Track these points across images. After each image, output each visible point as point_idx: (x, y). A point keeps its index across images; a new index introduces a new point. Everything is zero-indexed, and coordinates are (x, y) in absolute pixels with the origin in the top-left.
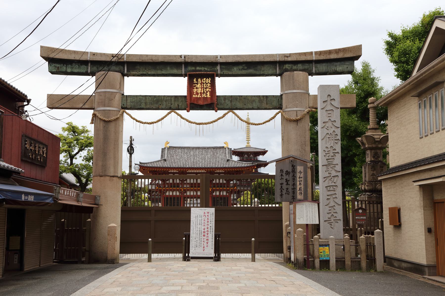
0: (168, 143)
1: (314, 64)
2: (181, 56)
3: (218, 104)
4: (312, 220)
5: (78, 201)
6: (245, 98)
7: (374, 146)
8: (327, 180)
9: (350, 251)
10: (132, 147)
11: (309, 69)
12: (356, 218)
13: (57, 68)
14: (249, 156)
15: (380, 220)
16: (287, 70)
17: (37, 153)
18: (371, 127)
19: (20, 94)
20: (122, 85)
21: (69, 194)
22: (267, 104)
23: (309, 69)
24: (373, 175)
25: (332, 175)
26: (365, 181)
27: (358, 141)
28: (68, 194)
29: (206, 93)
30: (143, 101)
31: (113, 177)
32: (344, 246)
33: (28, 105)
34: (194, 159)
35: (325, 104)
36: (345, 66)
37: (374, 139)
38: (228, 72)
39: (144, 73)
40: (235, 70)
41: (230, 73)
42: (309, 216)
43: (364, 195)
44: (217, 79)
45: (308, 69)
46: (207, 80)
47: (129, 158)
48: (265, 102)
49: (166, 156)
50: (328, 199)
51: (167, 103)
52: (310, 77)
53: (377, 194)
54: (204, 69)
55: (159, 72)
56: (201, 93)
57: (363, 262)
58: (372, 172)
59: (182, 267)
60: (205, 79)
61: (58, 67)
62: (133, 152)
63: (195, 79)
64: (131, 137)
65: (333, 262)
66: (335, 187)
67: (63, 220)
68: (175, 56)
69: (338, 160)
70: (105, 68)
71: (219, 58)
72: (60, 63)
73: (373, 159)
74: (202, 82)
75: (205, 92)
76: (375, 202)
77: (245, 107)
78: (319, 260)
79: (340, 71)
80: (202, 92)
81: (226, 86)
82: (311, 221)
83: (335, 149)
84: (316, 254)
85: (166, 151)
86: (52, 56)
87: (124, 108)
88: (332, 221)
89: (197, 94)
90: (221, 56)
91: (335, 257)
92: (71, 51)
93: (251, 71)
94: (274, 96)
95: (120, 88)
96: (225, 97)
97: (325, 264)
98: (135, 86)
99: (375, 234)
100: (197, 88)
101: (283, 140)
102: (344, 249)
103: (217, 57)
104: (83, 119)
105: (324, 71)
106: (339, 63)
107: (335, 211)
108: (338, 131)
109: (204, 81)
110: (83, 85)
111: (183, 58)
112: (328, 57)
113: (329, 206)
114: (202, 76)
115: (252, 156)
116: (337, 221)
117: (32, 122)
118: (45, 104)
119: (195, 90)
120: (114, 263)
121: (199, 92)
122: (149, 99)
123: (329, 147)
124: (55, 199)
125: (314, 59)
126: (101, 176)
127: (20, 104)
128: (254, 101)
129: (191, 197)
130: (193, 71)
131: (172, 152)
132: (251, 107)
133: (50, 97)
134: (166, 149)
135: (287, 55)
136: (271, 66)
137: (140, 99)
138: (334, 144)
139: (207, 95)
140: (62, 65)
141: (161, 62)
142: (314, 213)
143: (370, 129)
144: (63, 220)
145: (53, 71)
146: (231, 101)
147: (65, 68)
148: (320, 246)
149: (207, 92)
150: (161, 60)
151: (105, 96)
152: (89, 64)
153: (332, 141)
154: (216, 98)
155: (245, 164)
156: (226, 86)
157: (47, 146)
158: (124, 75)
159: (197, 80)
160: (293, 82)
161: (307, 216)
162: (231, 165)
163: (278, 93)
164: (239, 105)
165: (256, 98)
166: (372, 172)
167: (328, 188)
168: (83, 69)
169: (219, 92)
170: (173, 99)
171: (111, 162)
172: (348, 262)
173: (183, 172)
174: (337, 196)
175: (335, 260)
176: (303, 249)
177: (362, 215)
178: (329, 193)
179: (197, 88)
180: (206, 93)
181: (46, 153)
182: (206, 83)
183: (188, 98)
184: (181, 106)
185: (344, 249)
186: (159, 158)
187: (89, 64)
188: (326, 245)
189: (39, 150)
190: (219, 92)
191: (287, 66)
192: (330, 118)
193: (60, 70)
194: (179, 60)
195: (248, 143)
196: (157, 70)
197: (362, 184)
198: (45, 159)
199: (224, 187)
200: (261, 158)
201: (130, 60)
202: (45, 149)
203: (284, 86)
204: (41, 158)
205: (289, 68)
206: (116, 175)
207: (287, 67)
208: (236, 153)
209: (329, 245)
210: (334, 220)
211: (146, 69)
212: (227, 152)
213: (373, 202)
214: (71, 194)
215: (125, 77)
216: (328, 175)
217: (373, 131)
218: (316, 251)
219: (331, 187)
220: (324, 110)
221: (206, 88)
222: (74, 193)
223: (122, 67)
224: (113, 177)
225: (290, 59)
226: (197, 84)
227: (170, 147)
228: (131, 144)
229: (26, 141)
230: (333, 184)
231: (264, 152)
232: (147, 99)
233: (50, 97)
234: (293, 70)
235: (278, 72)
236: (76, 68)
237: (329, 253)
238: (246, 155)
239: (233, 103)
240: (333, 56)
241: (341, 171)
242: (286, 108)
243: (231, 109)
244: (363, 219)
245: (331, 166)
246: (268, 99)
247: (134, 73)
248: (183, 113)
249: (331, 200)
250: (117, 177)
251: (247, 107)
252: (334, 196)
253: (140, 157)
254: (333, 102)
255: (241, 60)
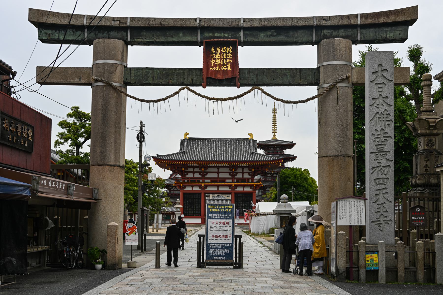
0: (187, 134)
1: (359, 29)
2: (196, 19)
3: (241, 79)
4: (358, 221)
5: (68, 195)
6: (273, 72)
7: (428, 131)
8: (376, 171)
9: (404, 258)
10: (143, 134)
11: (353, 36)
12: (413, 218)
13: (48, 35)
14: (275, 149)
15: (436, 220)
16: (325, 37)
17: (19, 135)
18: (425, 109)
19: (5, 67)
20: (125, 56)
21: (55, 186)
22: (301, 79)
23: (353, 36)
24: (426, 166)
25: (382, 165)
26: (417, 173)
27: (408, 125)
28: (54, 185)
29: (226, 65)
30: (149, 75)
31: (114, 166)
32: (396, 252)
33: (13, 78)
34: (216, 151)
35: (375, 76)
36: (398, 32)
37: (428, 123)
38: (254, 39)
39: (151, 40)
40: (262, 36)
41: (256, 40)
42: (353, 216)
43: (414, 190)
44: (239, 47)
45: (351, 36)
46: (228, 49)
47: (139, 146)
48: (299, 76)
49: (185, 148)
50: (376, 195)
51: (179, 77)
52: (353, 46)
53: (431, 189)
54: (224, 36)
55: (170, 39)
56: (220, 65)
57: (420, 272)
58: (425, 163)
59: (194, 276)
60: (225, 48)
61: (50, 34)
62: (144, 140)
63: (213, 48)
64: (141, 122)
65: (382, 273)
66: (385, 180)
67: (56, 217)
68: (189, 19)
69: (390, 146)
70: (105, 34)
71: (242, 21)
72: (52, 28)
73: (426, 148)
74: (221, 51)
75: (225, 64)
76: (426, 199)
77: (274, 82)
78: (365, 270)
79: (390, 38)
80: (222, 63)
81: (250, 57)
82: (356, 222)
83: (386, 133)
84: (362, 263)
85: (186, 143)
86: (43, 20)
87: (126, 84)
88: (382, 221)
89: (215, 66)
90: (245, 20)
91: (385, 266)
92: (64, 14)
93: (281, 38)
94: (309, 69)
95: (122, 58)
96: (249, 70)
97: (373, 274)
98: (140, 56)
99: (436, 238)
100: (215, 59)
101: (319, 122)
102: (396, 257)
103: (239, 20)
104: (82, 97)
105: (371, 38)
106: (389, 29)
107: (384, 210)
108: (391, 110)
109: (224, 50)
110: (81, 56)
111: (198, 21)
112: (376, 20)
113: (377, 203)
114: (222, 44)
115: (278, 149)
116: (387, 221)
117: (20, 100)
118: (35, 80)
119: (213, 61)
120: (115, 269)
121: (218, 63)
122: (157, 72)
123: (379, 129)
124: (34, 192)
125: (359, 22)
126: (99, 165)
127: (5, 77)
128: (285, 75)
129: (213, 193)
130: (211, 38)
131: (192, 144)
132: (281, 82)
133: (40, 70)
134: (186, 140)
135: (326, 18)
136: (307, 32)
137: (146, 72)
138: (385, 126)
139: (227, 67)
140: (54, 31)
141: (172, 27)
142: (359, 212)
143: (423, 111)
144: (56, 217)
145: (44, 38)
146: (257, 75)
147: (57, 35)
148: (367, 252)
149: (227, 64)
150: (171, 24)
151: (104, 69)
152: (86, 30)
153: (383, 123)
154: (238, 71)
155: (271, 158)
156: (250, 57)
157: (33, 128)
158: (127, 43)
159: (215, 50)
160: (334, 52)
161: (351, 216)
162: (256, 158)
163: (314, 65)
164: (267, 80)
165: (287, 71)
166: (425, 163)
167: (378, 180)
168: (77, 36)
169: (243, 64)
170: (186, 71)
171: (111, 149)
172: (401, 273)
173: (204, 166)
174: (388, 191)
175: (385, 270)
176: (345, 257)
177: (419, 214)
178: (378, 187)
179: (215, 59)
180: (226, 65)
181: (32, 137)
182: (226, 52)
183: (204, 71)
184: (196, 80)
185: (396, 257)
186: (178, 150)
187: (86, 30)
188: (374, 252)
189: (22, 132)
190: (243, 64)
191: (326, 32)
192: (381, 93)
193: (51, 38)
194: (194, 25)
195: (274, 135)
196: (167, 37)
197: (412, 178)
198: (31, 144)
199: (248, 182)
200: (288, 152)
201: (134, 24)
202: (30, 131)
203: (322, 56)
204: (24, 142)
205: (328, 35)
206: (118, 164)
207: (326, 34)
208: (261, 145)
209: (378, 251)
210: (384, 220)
211: (153, 35)
212: (251, 144)
213: (424, 198)
214: (57, 185)
215: (129, 47)
216: (378, 165)
217: (428, 113)
218: (361, 259)
219: (381, 180)
220: (374, 84)
221: (226, 59)
222: (62, 185)
223: (124, 34)
224: (114, 166)
225: (329, 23)
226: (216, 54)
227: (190, 138)
228: (141, 131)
229: (4, 120)
230: (384, 176)
231: (291, 145)
232: (155, 72)
233: (40, 70)
234: (332, 37)
235: (314, 40)
236: (70, 35)
237: (375, 260)
238: (272, 149)
239: (259, 78)
240: (382, 20)
241: (393, 159)
242: (324, 83)
243: (256, 85)
244: (420, 219)
245: (381, 154)
246: (302, 72)
247: (139, 40)
248: (198, 89)
249: (381, 196)
250: (119, 166)
251: (277, 83)
252: (384, 191)
253: (152, 149)
254: (385, 74)
255: (270, 24)
